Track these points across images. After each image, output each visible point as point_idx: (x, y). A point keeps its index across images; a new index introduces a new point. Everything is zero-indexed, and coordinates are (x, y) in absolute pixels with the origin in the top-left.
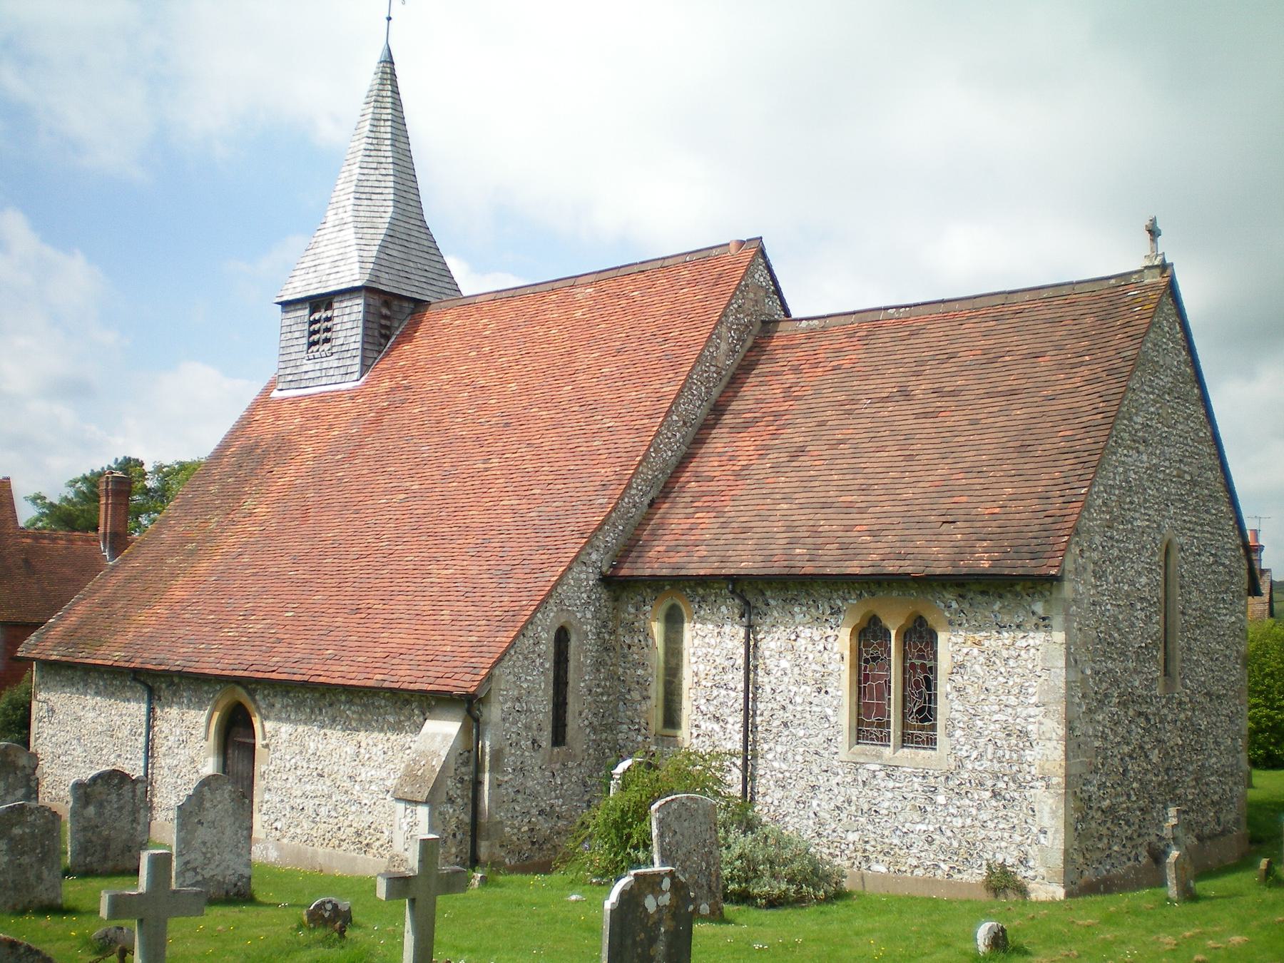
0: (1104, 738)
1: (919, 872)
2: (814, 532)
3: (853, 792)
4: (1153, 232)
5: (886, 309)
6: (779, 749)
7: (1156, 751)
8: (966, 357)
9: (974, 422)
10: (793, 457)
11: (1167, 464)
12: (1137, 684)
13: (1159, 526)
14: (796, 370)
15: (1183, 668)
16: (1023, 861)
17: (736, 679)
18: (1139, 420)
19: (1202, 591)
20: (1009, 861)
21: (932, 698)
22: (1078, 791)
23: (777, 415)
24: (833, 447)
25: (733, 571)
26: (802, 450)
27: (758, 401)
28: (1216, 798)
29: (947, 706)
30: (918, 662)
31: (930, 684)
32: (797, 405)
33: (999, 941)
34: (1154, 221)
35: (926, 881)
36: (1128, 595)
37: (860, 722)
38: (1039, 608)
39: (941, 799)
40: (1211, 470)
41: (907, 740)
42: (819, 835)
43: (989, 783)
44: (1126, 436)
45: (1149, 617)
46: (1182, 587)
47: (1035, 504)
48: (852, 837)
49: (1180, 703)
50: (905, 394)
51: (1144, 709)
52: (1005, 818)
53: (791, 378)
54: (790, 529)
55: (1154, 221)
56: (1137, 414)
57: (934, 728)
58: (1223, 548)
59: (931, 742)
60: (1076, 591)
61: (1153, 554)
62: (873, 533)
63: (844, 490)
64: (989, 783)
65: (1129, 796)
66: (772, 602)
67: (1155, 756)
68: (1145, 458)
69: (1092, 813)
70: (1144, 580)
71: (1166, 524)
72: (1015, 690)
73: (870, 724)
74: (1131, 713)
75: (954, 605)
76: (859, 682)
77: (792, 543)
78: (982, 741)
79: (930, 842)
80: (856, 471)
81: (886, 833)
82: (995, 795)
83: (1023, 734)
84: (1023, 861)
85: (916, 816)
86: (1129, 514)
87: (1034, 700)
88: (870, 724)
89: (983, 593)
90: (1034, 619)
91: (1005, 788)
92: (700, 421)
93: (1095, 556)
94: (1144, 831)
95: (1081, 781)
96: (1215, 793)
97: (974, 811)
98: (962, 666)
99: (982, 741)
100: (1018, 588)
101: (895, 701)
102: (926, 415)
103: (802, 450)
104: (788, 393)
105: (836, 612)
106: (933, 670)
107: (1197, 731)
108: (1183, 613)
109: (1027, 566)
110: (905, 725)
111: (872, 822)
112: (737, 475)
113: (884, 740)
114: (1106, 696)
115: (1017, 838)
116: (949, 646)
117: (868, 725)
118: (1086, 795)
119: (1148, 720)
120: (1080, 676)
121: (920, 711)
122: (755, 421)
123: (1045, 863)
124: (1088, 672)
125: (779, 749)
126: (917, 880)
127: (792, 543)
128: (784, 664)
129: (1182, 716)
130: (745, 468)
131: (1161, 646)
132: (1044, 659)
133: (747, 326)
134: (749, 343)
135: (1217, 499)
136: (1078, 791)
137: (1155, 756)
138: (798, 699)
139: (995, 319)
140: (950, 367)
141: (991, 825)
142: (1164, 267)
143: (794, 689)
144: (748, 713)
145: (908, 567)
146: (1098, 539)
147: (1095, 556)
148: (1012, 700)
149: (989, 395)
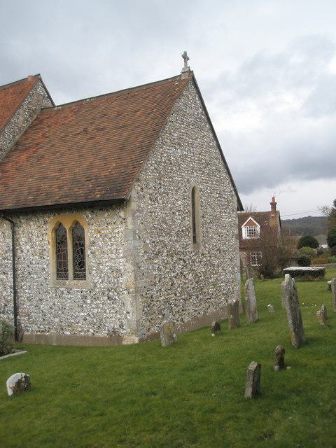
0: (159, 270)
1: (82, 334)
2: (38, 190)
3: (56, 300)
4: (185, 57)
5: (86, 99)
6: (28, 284)
7: (191, 274)
8: (111, 115)
9: (107, 139)
10: (39, 160)
11: (192, 154)
12: (178, 246)
13: (188, 180)
14: (49, 126)
15: (204, 240)
16: (121, 326)
17: (10, 254)
18: (176, 135)
19: (213, 208)
20: (116, 326)
21: (84, 258)
22: (144, 294)
23: (38, 144)
24: (54, 155)
25: (4, 208)
26: (43, 157)
27: (33, 139)
28: (224, 292)
29: (90, 261)
30: (78, 242)
31: (83, 251)
32: (45, 140)
33: (20, 388)
34: (185, 53)
35: (84, 337)
36: (171, 209)
37: (58, 270)
38: (122, 214)
39: (89, 301)
40: (217, 159)
41: (76, 277)
42: (44, 320)
43: (106, 293)
44: (168, 141)
45: (184, 218)
46: (202, 206)
47: (122, 170)
48: (57, 320)
49: (203, 254)
50: (86, 131)
51: (182, 257)
52: (114, 308)
53: (47, 129)
54: (30, 189)
55: (185, 53)
56: (174, 133)
57: (85, 270)
58: (224, 191)
59: (84, 277)
60: (139, 206)
61: (185, 192)
62: (59, 188)
63: (54, 171)
64: (106, 293)
65: (176, 295)
66: (23, 221)
67: (190, 277)
68: (179, 151)
69: (153, 303)
70: (180, 203)
71: (192, 180)
72: (114, 252)
73: (61, 271)
74: (175, 259)
75: (90, 216)
76: (57, 253)
77: (29, 194)
78: (103, 275)
79: (85, 320)
80: (59, 163)
81: (69, 317)
82: (109, 298)
83: (118, 270)
84: (121, 326)
85: (79, 309)
86: (170, 175)
87: (121, 255)
88: (61, 271)
89: (100, 210)
90: (121, 220)
91: (111, 294)
92: (9, 149)
93: (151, 191)
94: (185, 308)
95: (145, 290)
96: (224, 290)
97: (101, 306)
98: (94, 243)
99: (103, 275)
100: (114, 206)
101: (72, 259)
102: (91, 139)
103: (43, 157)
104: (44, 136)
105: (46, 223)
106: (83, 245)
107: (213, 265)
108: (203, 217)
109: (115, 196)
110: (75, 270)
111: (63, 313)
112: (17, 169)
113: (66, 277)
114: (159, 252)
115: (118, 316)
116: (90, 234)
117: (61, 272)
118: (149, 296)
119: (184, 261)
120: (143, 243)
121: (79, 264)
122: (29, 147)
123: (129, 326)
124: (148, 242)
125: (28, 284)
126: (81, 337)
127: (29, 194)
128: (28, 247)
129: (205, 259)
130: (21, 166)
131: (192, 231)
132: (125, 237)
133: (34, 111)
134: (35, 117)
135: (220, 171)
136: (144, 294)
137: (190, 277)
138: (34, 262)
139: (125, 99)
140: (104, 119)
141: (108, 311)
142: (191, 72)
143: (32, 258)
144: (15, 270)
145: (69, 200)
146: (151, 184)
147: (151, 191)
148: (114, 256)
149: (116, 128)
